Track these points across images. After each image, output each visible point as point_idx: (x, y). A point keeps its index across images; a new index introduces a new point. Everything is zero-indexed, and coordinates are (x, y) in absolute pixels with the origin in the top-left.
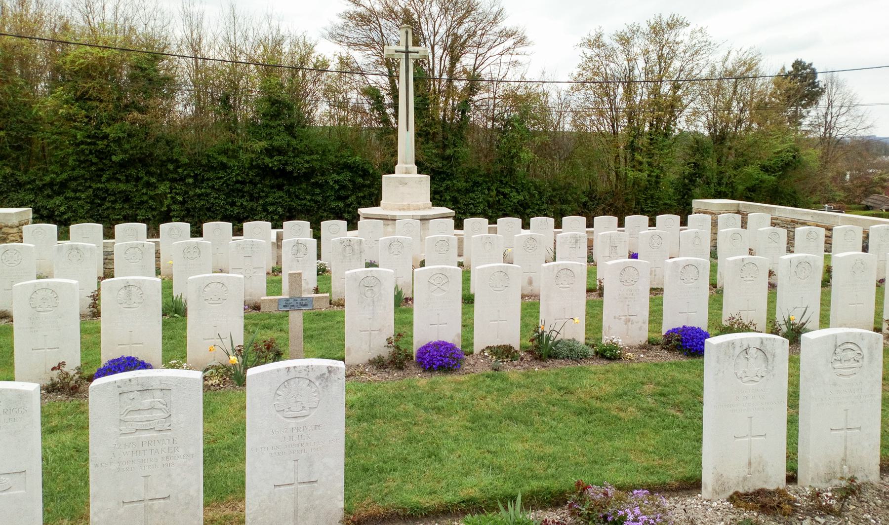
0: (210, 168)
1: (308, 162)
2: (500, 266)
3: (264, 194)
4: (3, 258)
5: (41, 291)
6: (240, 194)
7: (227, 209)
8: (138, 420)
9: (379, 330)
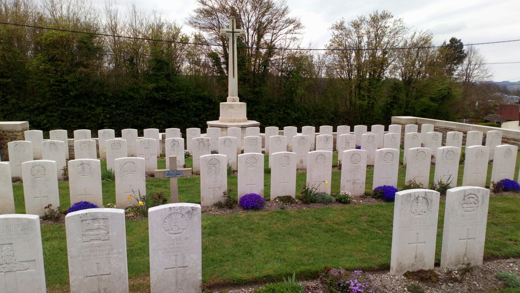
2: (285, 153)
3: (154, 114)
4: (15, 148)
7: (134, 122)
9: (219, 188)
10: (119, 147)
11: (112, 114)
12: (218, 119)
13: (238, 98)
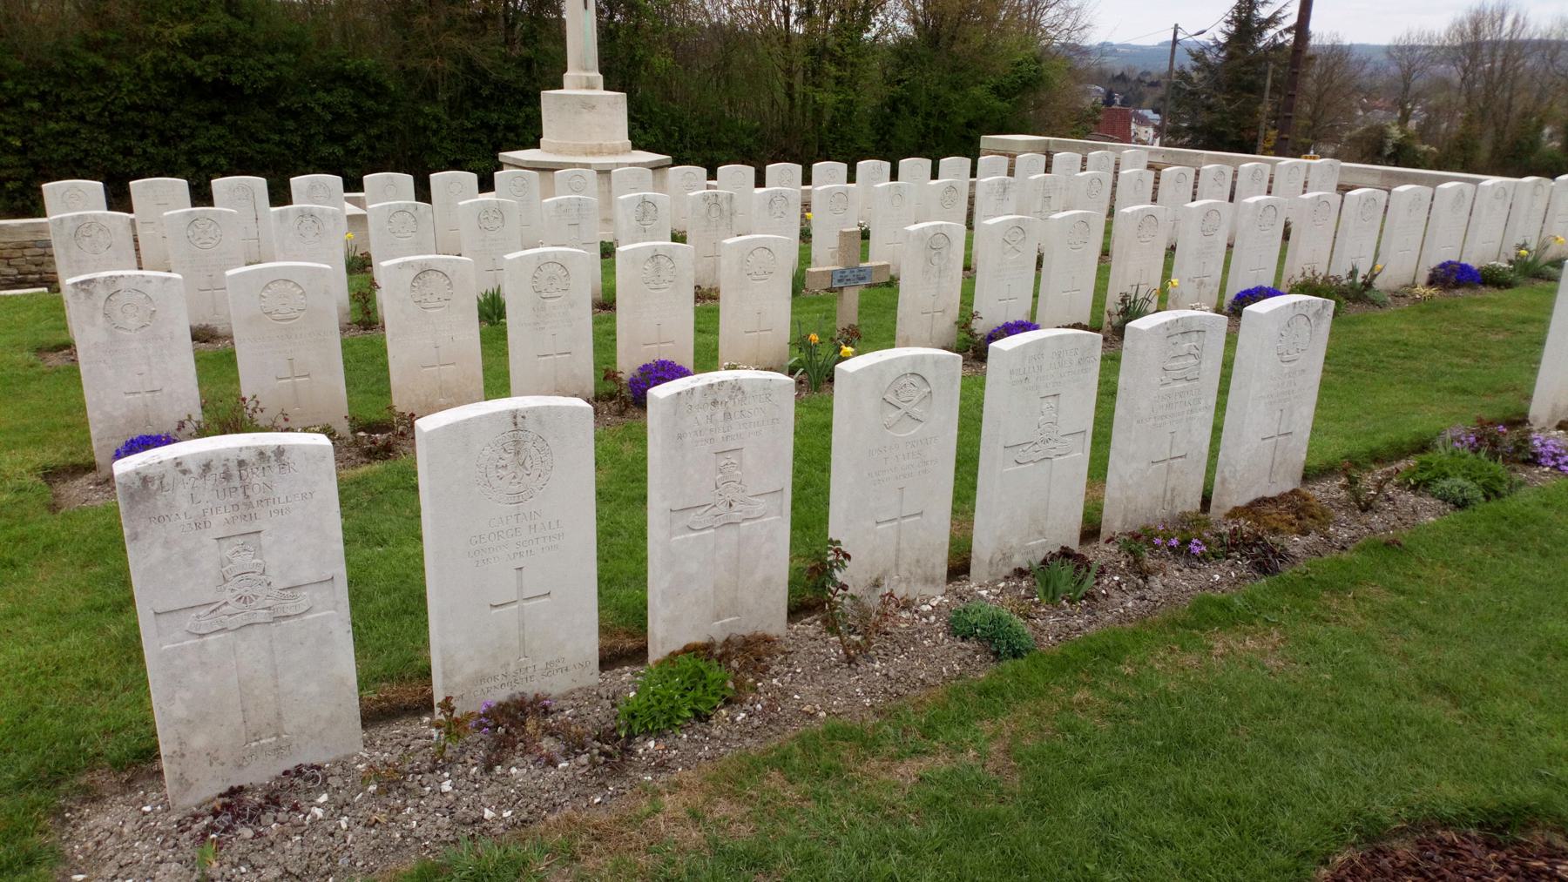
1: (270, 67)
4: (190, 233)
6: (138, 132)
7: (116, 163)
9: (943, 311)
10: (498, 223)
11: (29, 136)
12: (537, 145)
13: (601, 76)
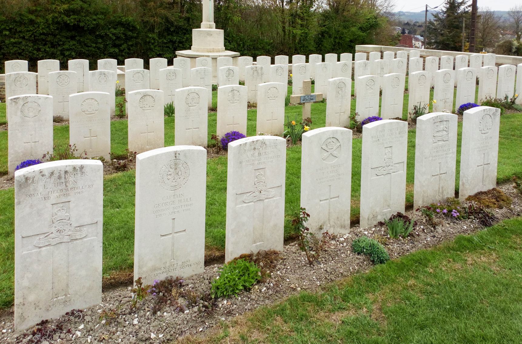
0: (21, 23)
1: (95, 20)
3: (61, 43)
4: (58, 80)
5: (191, 94)
6: (44, 43)
7: (34, 54)
8: (439, 136)
13: (215, 24)
